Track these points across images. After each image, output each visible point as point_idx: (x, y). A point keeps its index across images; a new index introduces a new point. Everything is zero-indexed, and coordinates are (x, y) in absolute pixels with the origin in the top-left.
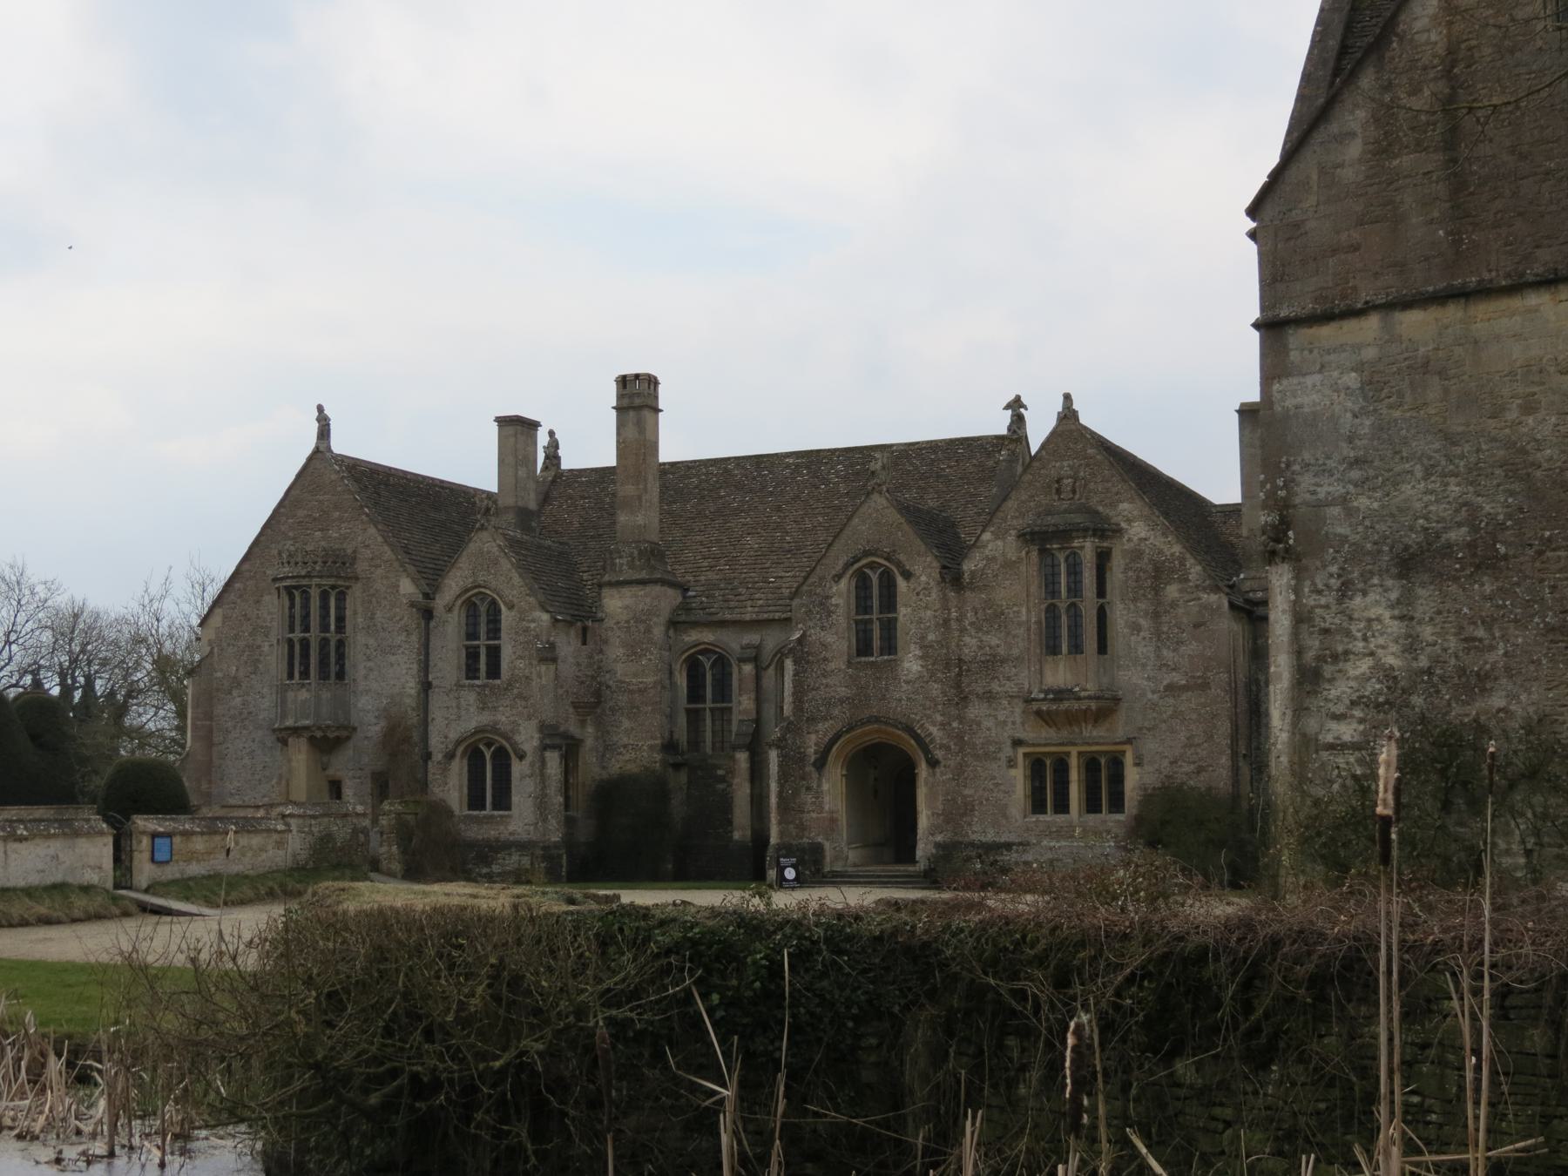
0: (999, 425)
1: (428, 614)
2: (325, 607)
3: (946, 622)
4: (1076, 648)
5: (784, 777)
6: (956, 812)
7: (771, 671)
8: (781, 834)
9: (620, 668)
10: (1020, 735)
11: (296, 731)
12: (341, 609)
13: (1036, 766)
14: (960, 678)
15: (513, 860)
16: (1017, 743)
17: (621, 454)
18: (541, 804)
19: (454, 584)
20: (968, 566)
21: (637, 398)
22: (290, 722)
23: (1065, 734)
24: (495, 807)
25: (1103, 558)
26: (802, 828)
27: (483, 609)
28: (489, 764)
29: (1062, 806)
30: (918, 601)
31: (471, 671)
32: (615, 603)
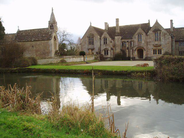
0: (147, 22)
1: (101, 39)
4: (158, 40)
11: (90, 49)
13: (154, 50)
14: (147, 43)
16: (152, 48)
19: (103, 36)
21: (117, 20)
25: (160, 33)
29: (156, 54)
31: (104, 43)
32: (116, 38)
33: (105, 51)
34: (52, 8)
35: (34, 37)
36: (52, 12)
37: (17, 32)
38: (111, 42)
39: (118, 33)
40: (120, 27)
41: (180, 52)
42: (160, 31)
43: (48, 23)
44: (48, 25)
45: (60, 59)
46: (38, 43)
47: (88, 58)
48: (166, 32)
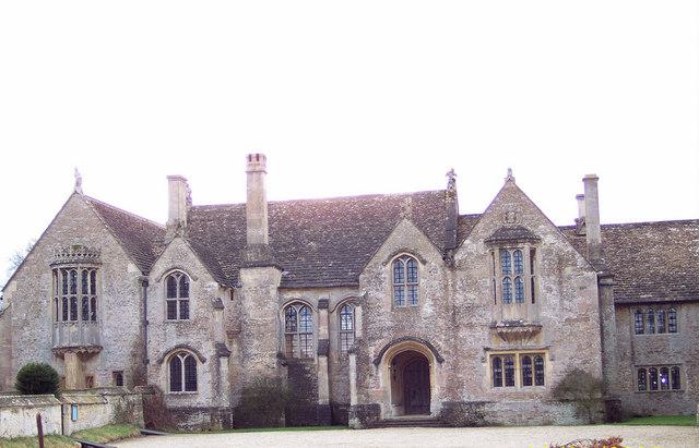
0: (441, 185)
1: (145, 283)
2: (84, 280)
3: (446, 286)
4: (520, 300)
5: (359, 370)
6: (453, 387)
7: (335, 313)
8: (359, 399)
9: (252, 314)
10: (487, 345)
11: (70, 349)
12: (93, 280)
13: (496, 362)
14: (454, 316)
15: (201, 418)
16: (487, 349)
17: (250, 197)
18: (217, 386)
19: (160, 267)
20: (458, 257)
21: (256, 163)
22: (65, 344)
23: (512, 345)
24: (187, 389)
25: (533, 252)
26: (367, 395)
27: (178, 280)
28: (184, 369)
29: (511, 383)
30: (431, 272)
31: (171, 314)
32: (248, 277)
41: (642, 371)
42: (534, 240)
48: (570, 249)
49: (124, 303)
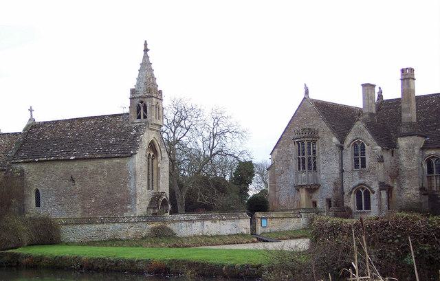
1: (342, 148)
2: (309, 147)
11: (302, 186)
19: (350, 138)
21: (407, 76)
22: (299, 184)
31: (356, 166)
32: (402, 142)
33: (359, 194)
34: (146, 44)
35: (78, 147)
36: (146, 57)
37: (28, 126)
38: (381, 160)
39: (411, 124)
40: (418, 98)
43: (128, 95)
44: (128, 103)
45: (150, 226)
46: (91, 166)
47: (274, 221)
49: (331, 160)
